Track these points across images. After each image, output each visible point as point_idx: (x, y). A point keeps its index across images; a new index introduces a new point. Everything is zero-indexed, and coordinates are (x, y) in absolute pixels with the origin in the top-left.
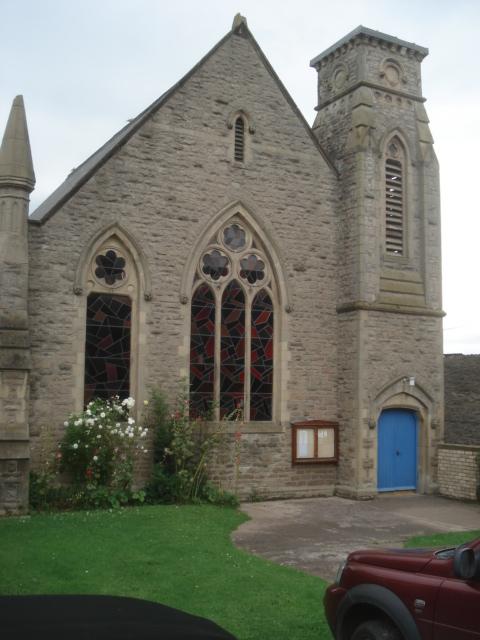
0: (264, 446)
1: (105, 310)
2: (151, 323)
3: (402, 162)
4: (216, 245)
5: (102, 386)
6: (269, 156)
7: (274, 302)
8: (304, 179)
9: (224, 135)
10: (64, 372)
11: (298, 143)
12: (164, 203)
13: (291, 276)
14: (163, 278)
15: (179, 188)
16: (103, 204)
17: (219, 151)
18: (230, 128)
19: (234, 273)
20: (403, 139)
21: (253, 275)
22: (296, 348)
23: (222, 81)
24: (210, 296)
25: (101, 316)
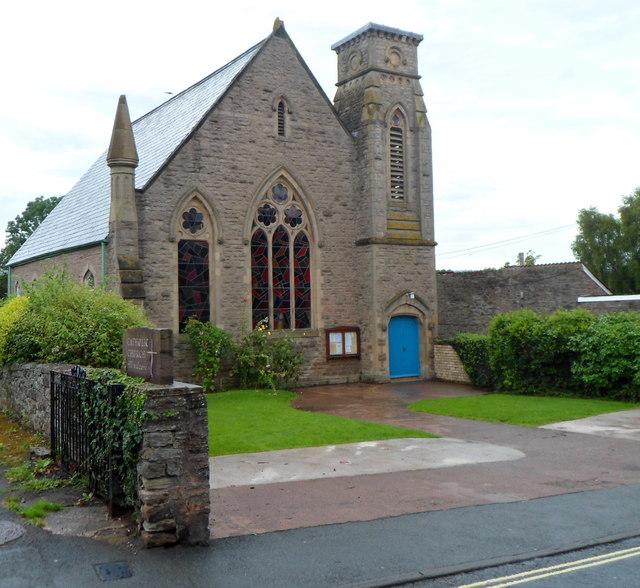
0: (306, 346)
1: (191, 252)
9: (270, 117)
13: (322, 220)
25: (188, 257)
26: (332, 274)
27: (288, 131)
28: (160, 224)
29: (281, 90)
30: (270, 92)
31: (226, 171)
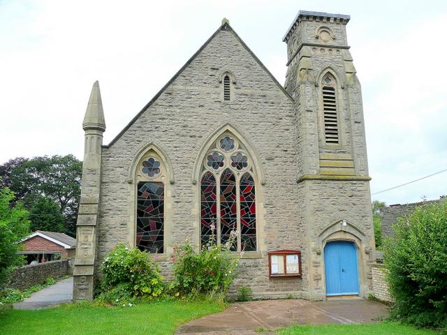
2: (174, 196)
9: (217, 87)
11: (265, 85)
13: (264, 163)
18: (221, 82)
19: (228, 164)
20: (333, 73)
24: (213, 179)
30: (218, 69)
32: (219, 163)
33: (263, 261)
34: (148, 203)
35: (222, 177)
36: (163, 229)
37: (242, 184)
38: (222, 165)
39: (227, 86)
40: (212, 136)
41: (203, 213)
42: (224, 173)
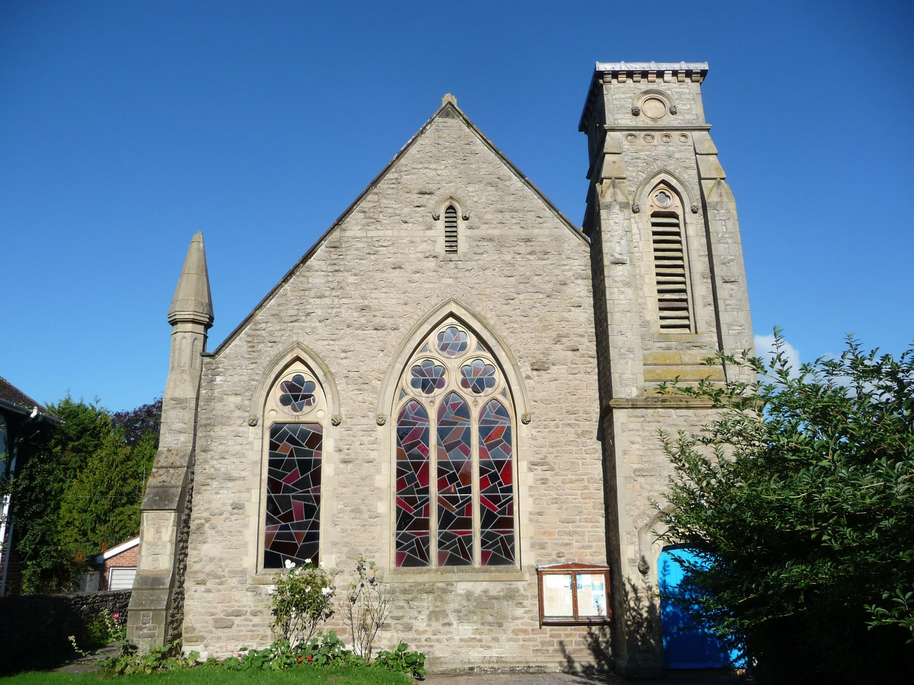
0: (497, 598)
1: (292, 440)
2: (341, 451)
3: (679, 212)
4: (428, 354)
5: (287, 527)
6: (491, 240)
7: (511, 412)
8: (540, 259)
9: (430, 228)
10: (236, 511)
11: (531, 217)
12: (356, 314)
13: (528, 377)
14: (355, 398)
15: (373, 296)
16: (284, 326)
17: (423, 247)
18: (437, 219)
19: (453, 381)
20: (674, 182)
21: (479, 386)
22: (539, 468)
23: (425, 171)
24: (422, 414)
25: (286, 448)
26: (552, 469)
27: (463, 245)
28: (238, 399)
29: (448, 189)
30: (431, 194)
31: (348, 315)
32: (434, 381)
33: (526, 585)
34: (290, 465)
35: (441, 412)
36: (318, 517)
37: (484, 422)
38: (441, 384)
39: (451, 224)
40: (421, 325)
41: (400, 485)
42: (446, 400)
